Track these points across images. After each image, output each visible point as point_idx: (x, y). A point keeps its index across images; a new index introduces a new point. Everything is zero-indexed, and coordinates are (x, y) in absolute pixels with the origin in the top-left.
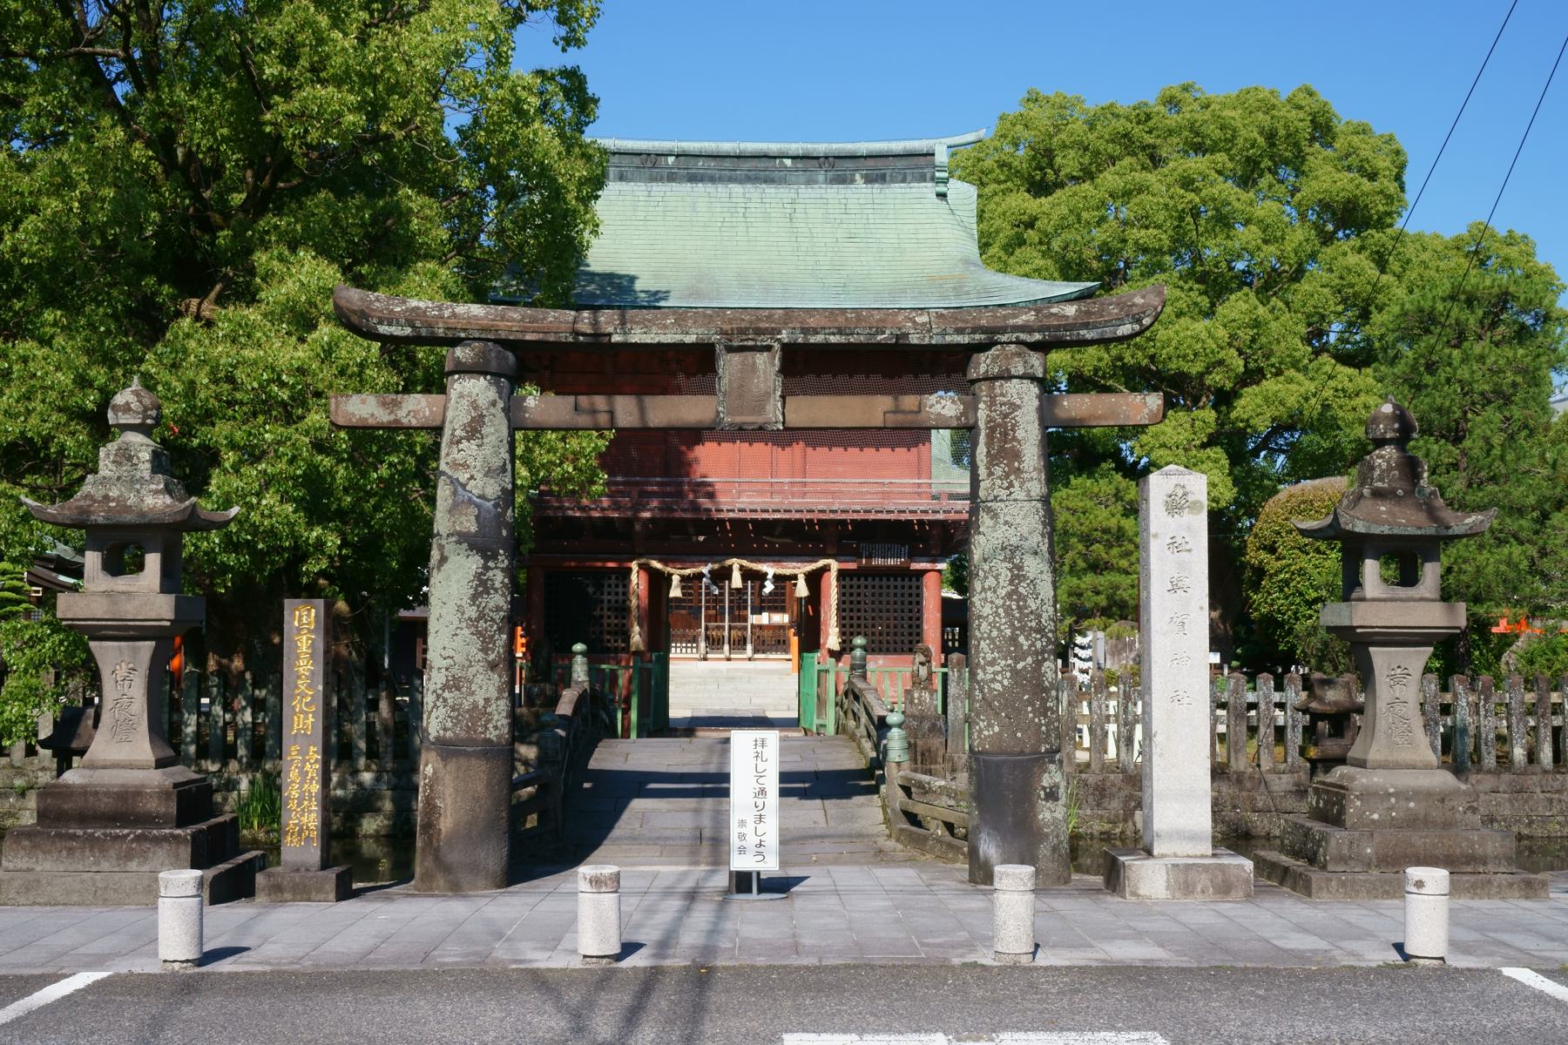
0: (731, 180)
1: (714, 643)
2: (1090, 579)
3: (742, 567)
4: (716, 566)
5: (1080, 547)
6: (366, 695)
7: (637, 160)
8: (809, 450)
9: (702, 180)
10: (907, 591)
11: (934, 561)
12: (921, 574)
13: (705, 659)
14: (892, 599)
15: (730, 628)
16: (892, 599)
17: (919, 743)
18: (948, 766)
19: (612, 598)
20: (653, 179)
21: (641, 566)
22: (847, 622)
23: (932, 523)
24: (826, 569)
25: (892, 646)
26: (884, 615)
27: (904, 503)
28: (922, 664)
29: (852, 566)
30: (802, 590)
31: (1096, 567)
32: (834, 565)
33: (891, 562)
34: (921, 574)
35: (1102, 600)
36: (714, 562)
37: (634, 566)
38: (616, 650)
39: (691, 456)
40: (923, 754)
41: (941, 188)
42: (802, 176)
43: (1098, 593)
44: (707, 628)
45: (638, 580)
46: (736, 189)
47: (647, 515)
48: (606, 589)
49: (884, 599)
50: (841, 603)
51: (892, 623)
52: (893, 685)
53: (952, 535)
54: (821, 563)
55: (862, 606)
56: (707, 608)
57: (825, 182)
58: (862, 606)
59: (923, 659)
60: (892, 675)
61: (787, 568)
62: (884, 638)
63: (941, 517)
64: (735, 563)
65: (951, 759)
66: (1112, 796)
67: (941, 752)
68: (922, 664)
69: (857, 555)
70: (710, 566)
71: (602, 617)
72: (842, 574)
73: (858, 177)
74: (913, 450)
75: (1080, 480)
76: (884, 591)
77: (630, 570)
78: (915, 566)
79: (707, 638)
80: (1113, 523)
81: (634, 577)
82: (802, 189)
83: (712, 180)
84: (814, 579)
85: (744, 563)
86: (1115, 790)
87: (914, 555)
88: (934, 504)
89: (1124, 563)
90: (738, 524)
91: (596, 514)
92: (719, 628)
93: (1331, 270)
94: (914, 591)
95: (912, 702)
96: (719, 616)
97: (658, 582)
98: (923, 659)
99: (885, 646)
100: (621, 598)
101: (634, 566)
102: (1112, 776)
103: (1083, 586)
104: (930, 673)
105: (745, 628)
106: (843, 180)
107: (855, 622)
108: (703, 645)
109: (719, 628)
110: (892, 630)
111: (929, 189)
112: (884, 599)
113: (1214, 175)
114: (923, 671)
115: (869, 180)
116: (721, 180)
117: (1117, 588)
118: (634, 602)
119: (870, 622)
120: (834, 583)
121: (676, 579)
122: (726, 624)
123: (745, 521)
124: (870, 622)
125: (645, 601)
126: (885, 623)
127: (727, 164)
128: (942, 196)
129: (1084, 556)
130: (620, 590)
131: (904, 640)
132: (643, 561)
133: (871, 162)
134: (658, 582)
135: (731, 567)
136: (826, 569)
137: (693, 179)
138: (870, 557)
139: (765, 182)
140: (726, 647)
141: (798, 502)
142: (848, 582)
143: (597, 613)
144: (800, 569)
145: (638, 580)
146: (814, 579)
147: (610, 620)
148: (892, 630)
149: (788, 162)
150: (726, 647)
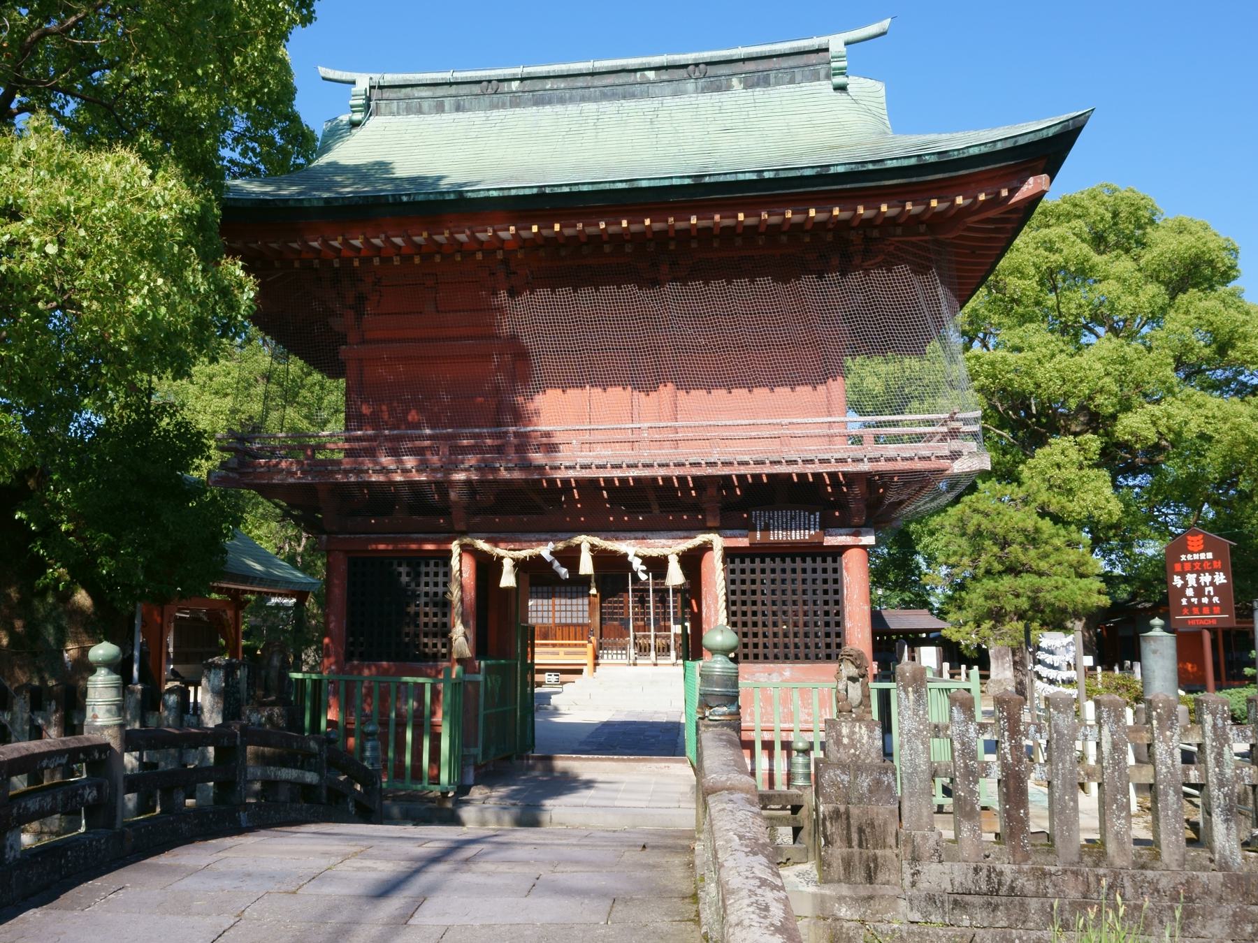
0: (583, 99)
1: (643, 650)
2: (1007, 581)
3: (593, 548)
4: (561, 545)
5: (996, 549)
6: (12, 722)
7: (476, 89)
8: (682, 393)
9: (550, 102)
10: (820, 576)
11: (856, 534)
12: (840, 551)
13: (635, 665)
14: (799, 587)
15: (656, 637)
16: (799, 587)
17: (854, 811)
18: (905, 851)
19: (431, 589)
20: (494, 106)
21: (465, 548)
22: (739, 618)
23: (851, 478)
24: (706, 548)
25: (833, 609)
26: (790, 608)
27: (814, 449)
28: (853, 679)
29: (743, 542)
30: (675, 576)
31: (1014, 570)
32: (718, 542)
33: (796, 536)
34: (840, 551)
35: (1024, 603)
36: (555, 541)
37: (455, 547)
38: (435, 657)
39: (531, 406)
40: (861, 831)
41: (839, 80)
42: (668, 88)
43: (1017, 596)
44: (635, 638)
45: (462, 567)
46: (590, 107)
47: (460, 476)
48: (424, 579)
49: (789, 587)
50: (730, 593)
51: (801, 619)
52: (806, 704)
53: (883, 496)
54: (701, 539)
55: (758, 597)
56: (636, 620)
57: (696, 91)
58: (758, 597)
59: (853, 671)
60: (804, 692)
61: (659, 546)
62: (791, 640)
63: (865, 467)
64: (585, 541)
65: (910, 840)
66: (1207, 915)
67: (892, 828)
68: (853, 679)
69: (749, 527)
70: (551, 546)
71: (417, 614)
72: (730, 555)
73: (735, 81)
74: (821, 388)
75: (988, 484)
76: (789, 576)
77: (449, 554)
78: (830, 541)
79: (635, 644)
80: (1029, 525)
81: (455, 562)
82: (669, 101)
83: (562, 101)
84: (692, 561)
85: (597, 541)
86: (1210, 902)
87: (827, 525)
88: (857, 451)
89: (1043, 565)
90: (589, 486)
91: (398, 478)
92: (644, 637)
93: (1187, 312)
94: (830, 576)
95: (838, 742)
96: (646, 627)
97: (488, 568)
98: (853, 671)
99: (792, 651)
100: (440, 589)
101: (455, 547)
102: (1204, 876)
103: (1001, 588)
104: (866, 696)
105: (669, 637)
106: (718, 87)
107: (749, 618)
108: (632, 651)
109: (644, 637)
110: (801, 630)
111: (826, 87)
112: (789, 587)
113: (1073, 238)
114: (855, 691)
115: (748, 85)
116: (572, 100)
117: (1038, 590)
118: (456, 593)
119: (770, 619)
120: (719, 565)
121: (508, 565)
122: (652, 633)
123: (594, 481)
124: (770, 619)
125: (471, 594)
126: (791, 619)
127: (580, 82)
128: (841, 88)
129: (1000, 560)
130: (441, 579)
131: (823, 643)
132: (467, 540)
133: (751, 66)
134: (488, 568)
135: (579, 546)
136: (706, 548)
137: (539, 102)
138: (766, 529)
139: (624, 98)
140: (653, 653)
141: (665, 453)
142: (738, 565)
143: (412, 609)
144: (671, 547)
145: (462, 567)
146: (692, 561)
147: (428, 617)
148: (801, 630)
149: (651, 75)
150: (653, 653)
